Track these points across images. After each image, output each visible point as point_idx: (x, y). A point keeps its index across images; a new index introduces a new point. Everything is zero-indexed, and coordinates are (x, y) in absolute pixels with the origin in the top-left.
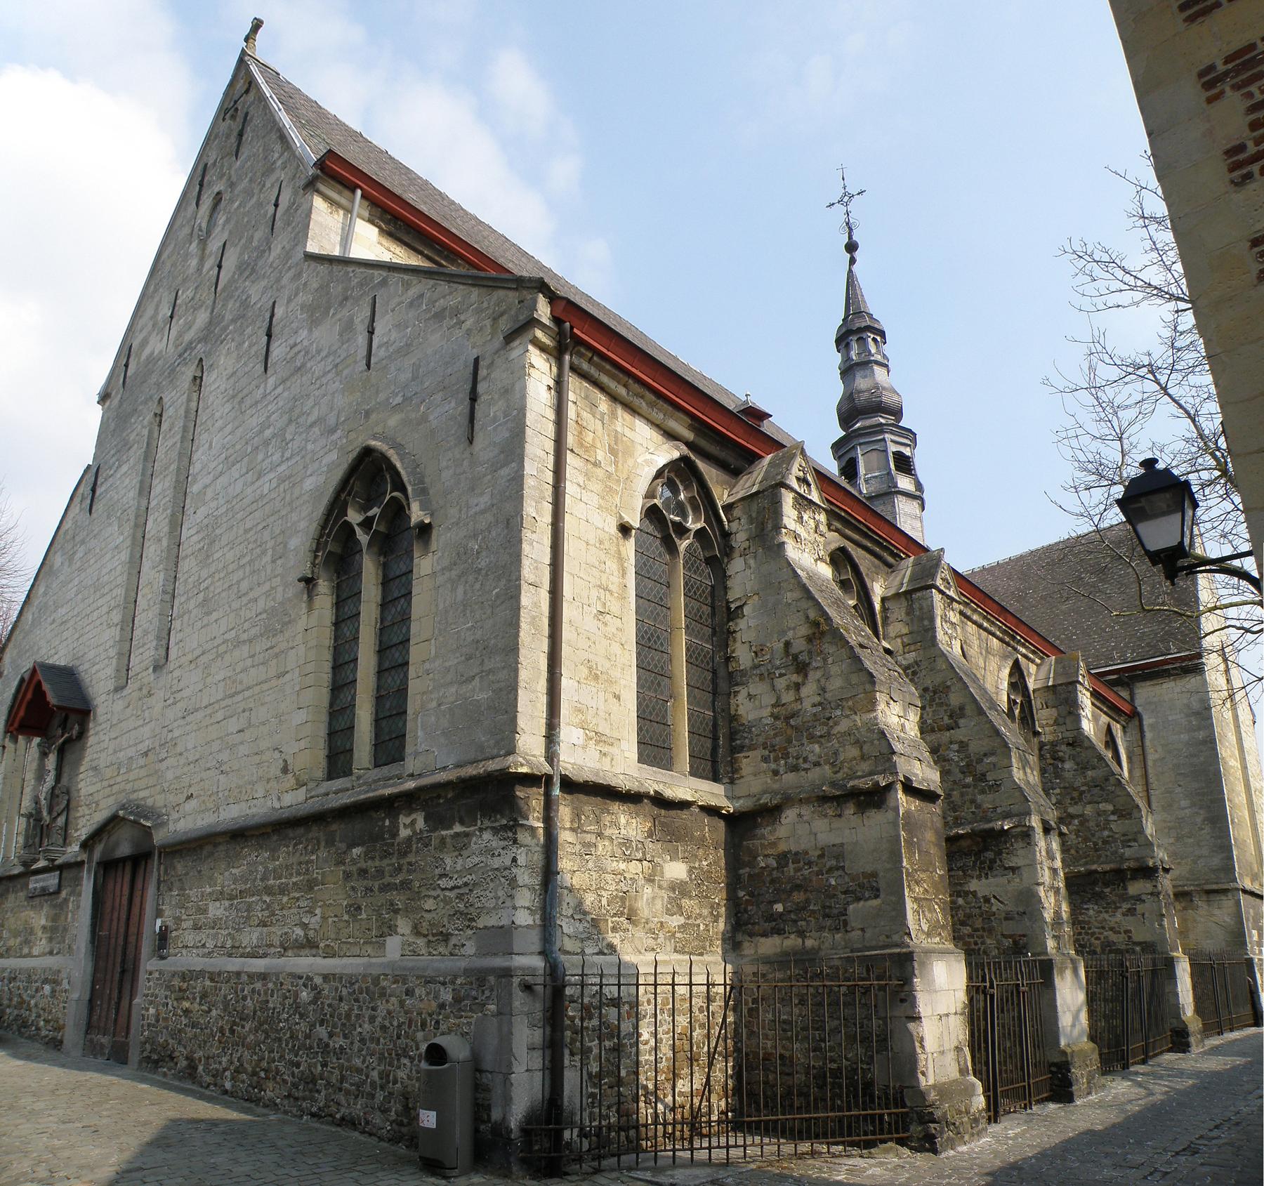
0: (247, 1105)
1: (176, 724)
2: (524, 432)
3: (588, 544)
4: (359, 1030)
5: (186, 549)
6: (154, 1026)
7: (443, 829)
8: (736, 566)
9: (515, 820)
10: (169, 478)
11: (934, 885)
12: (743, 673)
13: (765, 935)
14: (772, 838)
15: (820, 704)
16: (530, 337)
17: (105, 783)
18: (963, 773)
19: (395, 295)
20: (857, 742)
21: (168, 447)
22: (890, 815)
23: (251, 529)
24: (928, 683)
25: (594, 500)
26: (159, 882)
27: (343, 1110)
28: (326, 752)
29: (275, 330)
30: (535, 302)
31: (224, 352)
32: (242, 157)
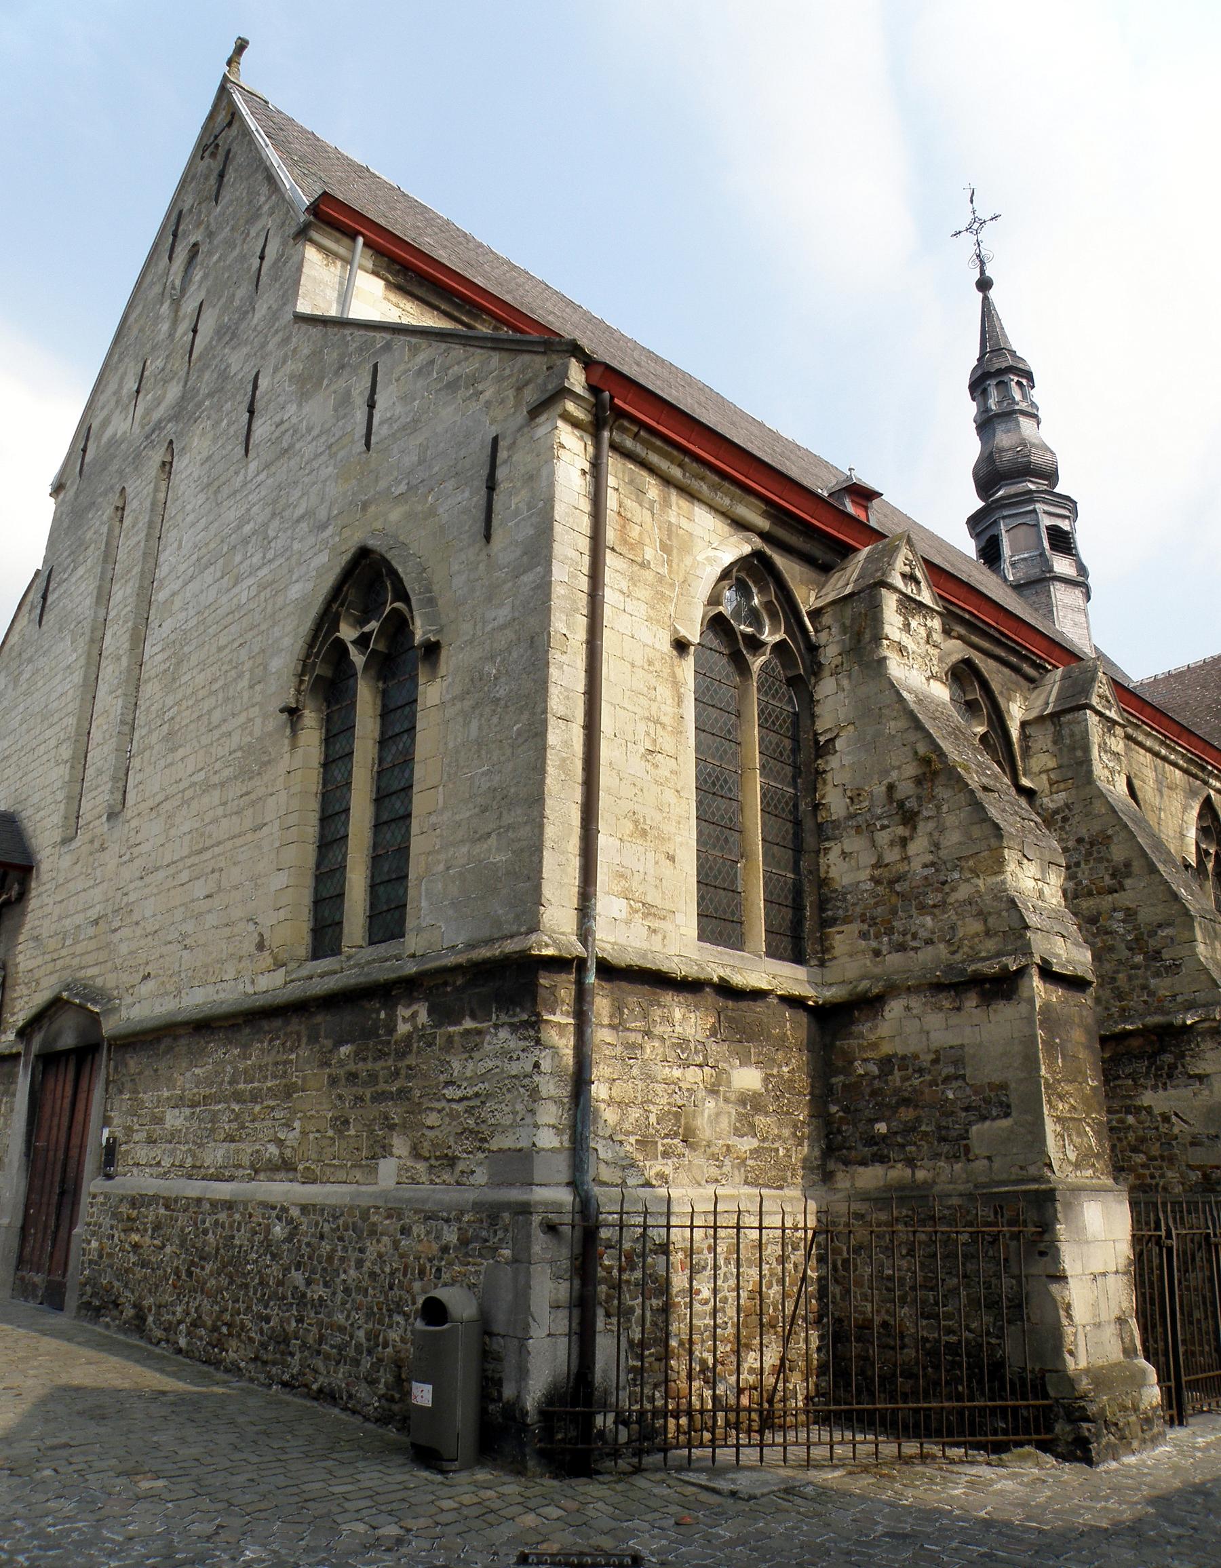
0: (205, 1368)
1: (132, 886)
2: (552, 529)
3: (633, 665)
4: (343, 1276)
5: (149, 671)
6: (96, 1263)
7: (451, 1024)
8: (826, 688)
9: (538, 1015)
10: (131, 584)
11: (1085, 1100)
12: (836, 824)
13: (863, 1163)
14: (873, 1037)
15: (933, 864)
16: (559, 410)
17: (48, 957)
18: (1130, 949)
19: (400, 365)
20: (980, 913)
21: (130, 545)
22: (1023, 1008)
23: (226, 646)
24: (1083, 832)
25: (641, 610)
26: (108, 1083)
27: (321, 1379)
28: (310, 925)
29: (259, 405)
30: (566, 368)
31: (198, 432)
32: (224, 201)
